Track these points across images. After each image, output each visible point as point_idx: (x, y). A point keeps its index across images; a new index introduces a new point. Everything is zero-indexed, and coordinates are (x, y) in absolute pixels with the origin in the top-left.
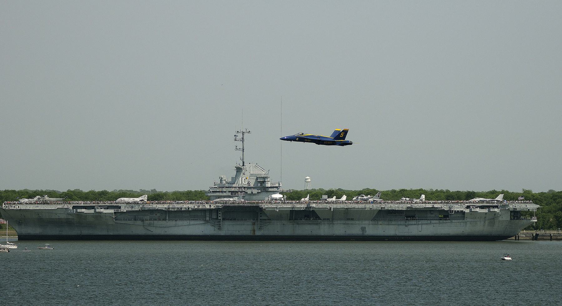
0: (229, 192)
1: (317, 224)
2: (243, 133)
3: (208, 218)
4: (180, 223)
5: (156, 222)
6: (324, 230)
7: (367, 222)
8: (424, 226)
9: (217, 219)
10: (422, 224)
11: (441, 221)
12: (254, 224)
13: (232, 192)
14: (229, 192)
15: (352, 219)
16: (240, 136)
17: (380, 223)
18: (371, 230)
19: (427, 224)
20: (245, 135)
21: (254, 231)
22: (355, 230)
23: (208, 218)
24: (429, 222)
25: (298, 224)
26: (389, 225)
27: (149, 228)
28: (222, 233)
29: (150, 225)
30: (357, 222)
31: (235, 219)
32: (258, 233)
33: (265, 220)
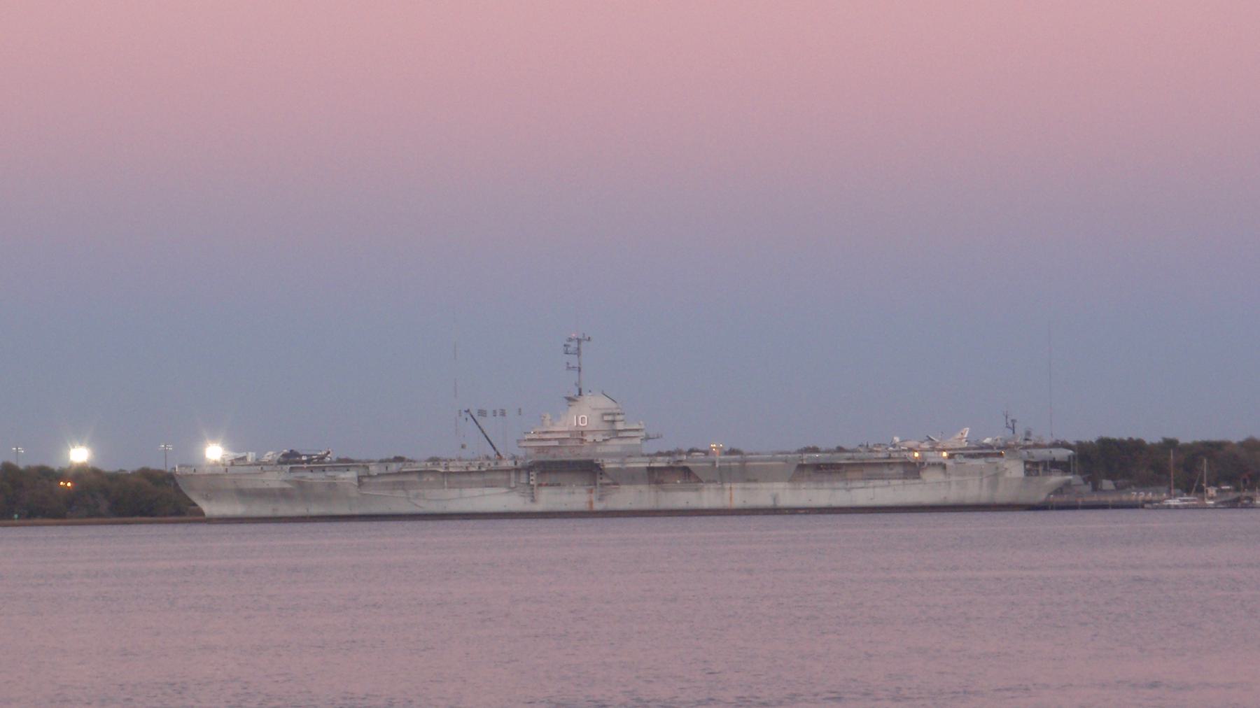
1: (697, 490)
2: (579, 341)
3: (513, 485)
4: (467, 492)
6: (709, 497)
7: (781, 485)
8: (877, 490)
15: (755, 481)
16: (574, 345)
17: (803, 486)
18: (788, 495)
19: (882, 487)
20: (584, 344)
22: (762, 495)
23: (513, 485)
24: (886, 482)
25: (663, 490)
28: (538, 507)
29: (417, 496)
30: (764, 485)
31: (559, 485)
32: (598, 506)
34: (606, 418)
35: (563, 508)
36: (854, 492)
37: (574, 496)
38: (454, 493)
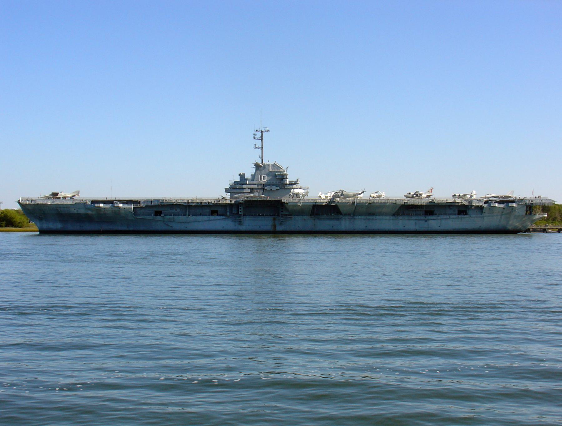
0: (249, 188)
1: (338, 219)
2: (262, 132)
3: (228, 214)
5: (175, 217)
8: (443, 221)
9: (238, 214)
10: (441, 219)
11: (460, 216)
12: (274, 219)
14: (249, 188)
19: (445, 219)
20: (264, 134)
21: (275, 226)
23: (228, 214)
26: (409, 219)
27: (169, 224)
28: (243, 228)
32: (279, 228)
33: (286, 215)
35: (426, 229)
36: (430, 222)
37: (265, 223)
38: (192, 218)
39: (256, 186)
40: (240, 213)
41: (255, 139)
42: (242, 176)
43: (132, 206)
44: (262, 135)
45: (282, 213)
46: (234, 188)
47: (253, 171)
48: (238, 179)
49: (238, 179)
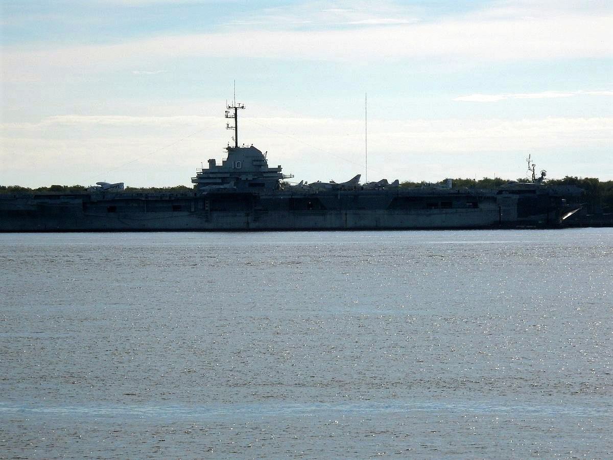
0: (219, 178)
10: (446, 213)
13: (223, 179)
15: (364, 208)
21: (248, 223)
23: (193, 210)
33: (261, 210)
34: (255, 163)
39: (228, 175)
40: (206, 209)
41: (227, 117)
42: (212, 162)
43: (80, 201)
44: (236, 114)
45: (256, 208)
46: (203, 178)
47: (225, 156)
48: (207, 166)
49: (207, 166)
